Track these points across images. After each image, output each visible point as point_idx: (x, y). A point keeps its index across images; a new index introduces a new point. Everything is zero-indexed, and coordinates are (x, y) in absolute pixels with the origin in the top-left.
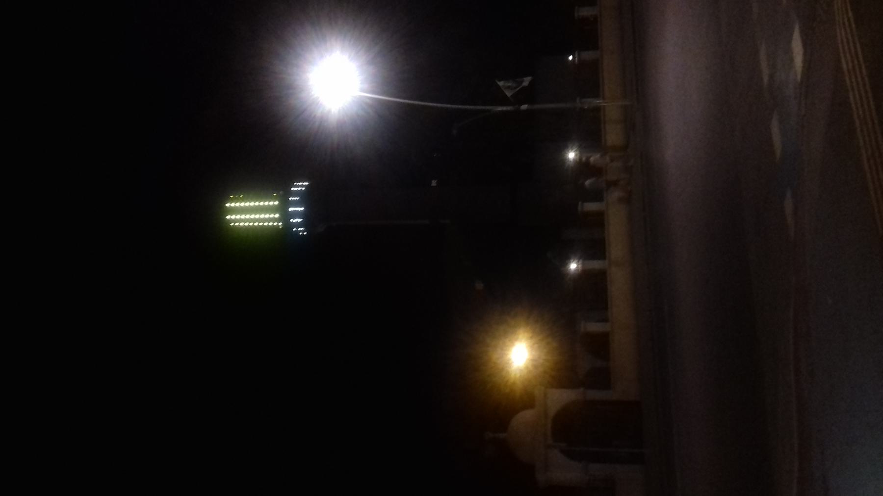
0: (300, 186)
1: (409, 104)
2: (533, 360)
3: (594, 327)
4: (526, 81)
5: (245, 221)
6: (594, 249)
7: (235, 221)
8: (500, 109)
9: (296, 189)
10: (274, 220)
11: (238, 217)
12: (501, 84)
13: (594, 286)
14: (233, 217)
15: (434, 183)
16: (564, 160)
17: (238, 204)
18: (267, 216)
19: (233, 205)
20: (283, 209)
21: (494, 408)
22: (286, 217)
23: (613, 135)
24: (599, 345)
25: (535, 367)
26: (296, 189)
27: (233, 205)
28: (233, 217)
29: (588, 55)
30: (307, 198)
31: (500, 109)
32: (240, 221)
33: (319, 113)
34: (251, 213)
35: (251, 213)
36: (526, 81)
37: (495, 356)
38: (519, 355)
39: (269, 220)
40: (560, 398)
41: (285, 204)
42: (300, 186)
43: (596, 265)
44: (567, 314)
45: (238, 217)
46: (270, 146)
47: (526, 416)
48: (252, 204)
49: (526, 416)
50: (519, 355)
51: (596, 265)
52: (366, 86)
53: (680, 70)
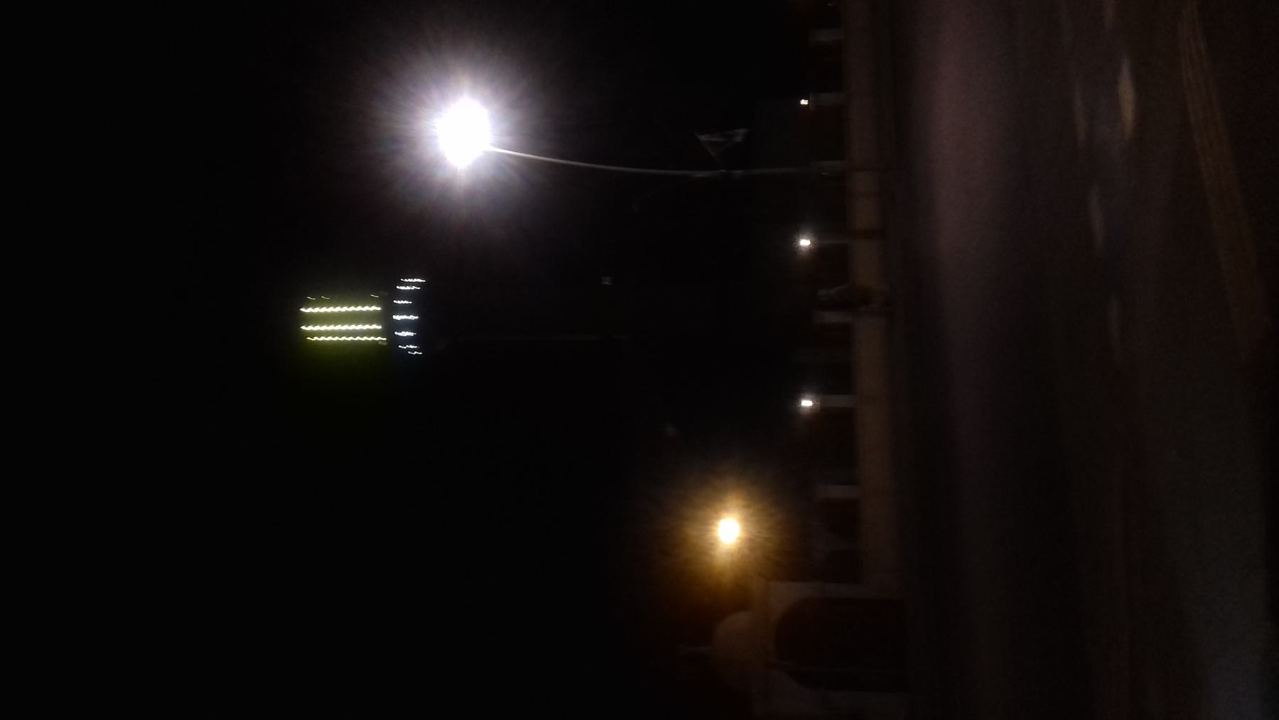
0: (411, 284)
1: (563, 165)
2: (751, 540)
3: (837, 492)
4: (740, 134)
5: (327, 334)
6: (834, 379)
7: (313, 334)
8: (700, 174)
9: (402, 288)
10: (375, 333)
11: (317, 328)
12: (703, 138)
13: (835, 428)
14: (310, 328)
15: (607, 282)
16: (794, 250)
17: (317, 310)
18: (367, 327)
19: (309, 310)
20: (384, 317)
21: (692, 605)
22: (390, 328)
23: (864, 213)
24: (843, 518)
25: (752, 549)
26: (402, 288)
27: (309, 310)
28: (310, 328)
29: (829, 99)
30: (420, 301)
31: (700, 174)
32: (319, 334)
33: (440, 175)
34: (338, 323)
35: (338, 323)
36: (740, 134)
37: (692, 531)
38: (729, 531)
39: (369, 333)
40: (786, 594)
41: (390, 309)
42: (411, 284)
43: (840, 401)
44: (793, 473)
45: (317, 328)
46: (375, 224)
47: (740, 620)
48: (345, 309)
49: (740, 620)
50: (729, 531)
51: (840, 401)
52: (507, 139)
53: (961, 114)
